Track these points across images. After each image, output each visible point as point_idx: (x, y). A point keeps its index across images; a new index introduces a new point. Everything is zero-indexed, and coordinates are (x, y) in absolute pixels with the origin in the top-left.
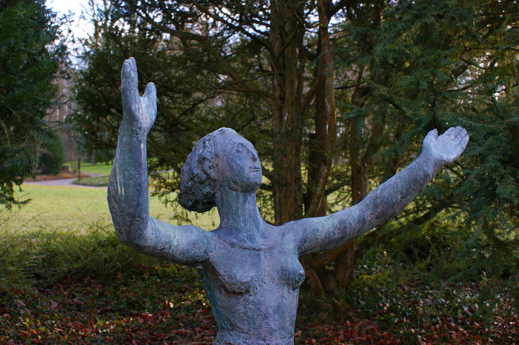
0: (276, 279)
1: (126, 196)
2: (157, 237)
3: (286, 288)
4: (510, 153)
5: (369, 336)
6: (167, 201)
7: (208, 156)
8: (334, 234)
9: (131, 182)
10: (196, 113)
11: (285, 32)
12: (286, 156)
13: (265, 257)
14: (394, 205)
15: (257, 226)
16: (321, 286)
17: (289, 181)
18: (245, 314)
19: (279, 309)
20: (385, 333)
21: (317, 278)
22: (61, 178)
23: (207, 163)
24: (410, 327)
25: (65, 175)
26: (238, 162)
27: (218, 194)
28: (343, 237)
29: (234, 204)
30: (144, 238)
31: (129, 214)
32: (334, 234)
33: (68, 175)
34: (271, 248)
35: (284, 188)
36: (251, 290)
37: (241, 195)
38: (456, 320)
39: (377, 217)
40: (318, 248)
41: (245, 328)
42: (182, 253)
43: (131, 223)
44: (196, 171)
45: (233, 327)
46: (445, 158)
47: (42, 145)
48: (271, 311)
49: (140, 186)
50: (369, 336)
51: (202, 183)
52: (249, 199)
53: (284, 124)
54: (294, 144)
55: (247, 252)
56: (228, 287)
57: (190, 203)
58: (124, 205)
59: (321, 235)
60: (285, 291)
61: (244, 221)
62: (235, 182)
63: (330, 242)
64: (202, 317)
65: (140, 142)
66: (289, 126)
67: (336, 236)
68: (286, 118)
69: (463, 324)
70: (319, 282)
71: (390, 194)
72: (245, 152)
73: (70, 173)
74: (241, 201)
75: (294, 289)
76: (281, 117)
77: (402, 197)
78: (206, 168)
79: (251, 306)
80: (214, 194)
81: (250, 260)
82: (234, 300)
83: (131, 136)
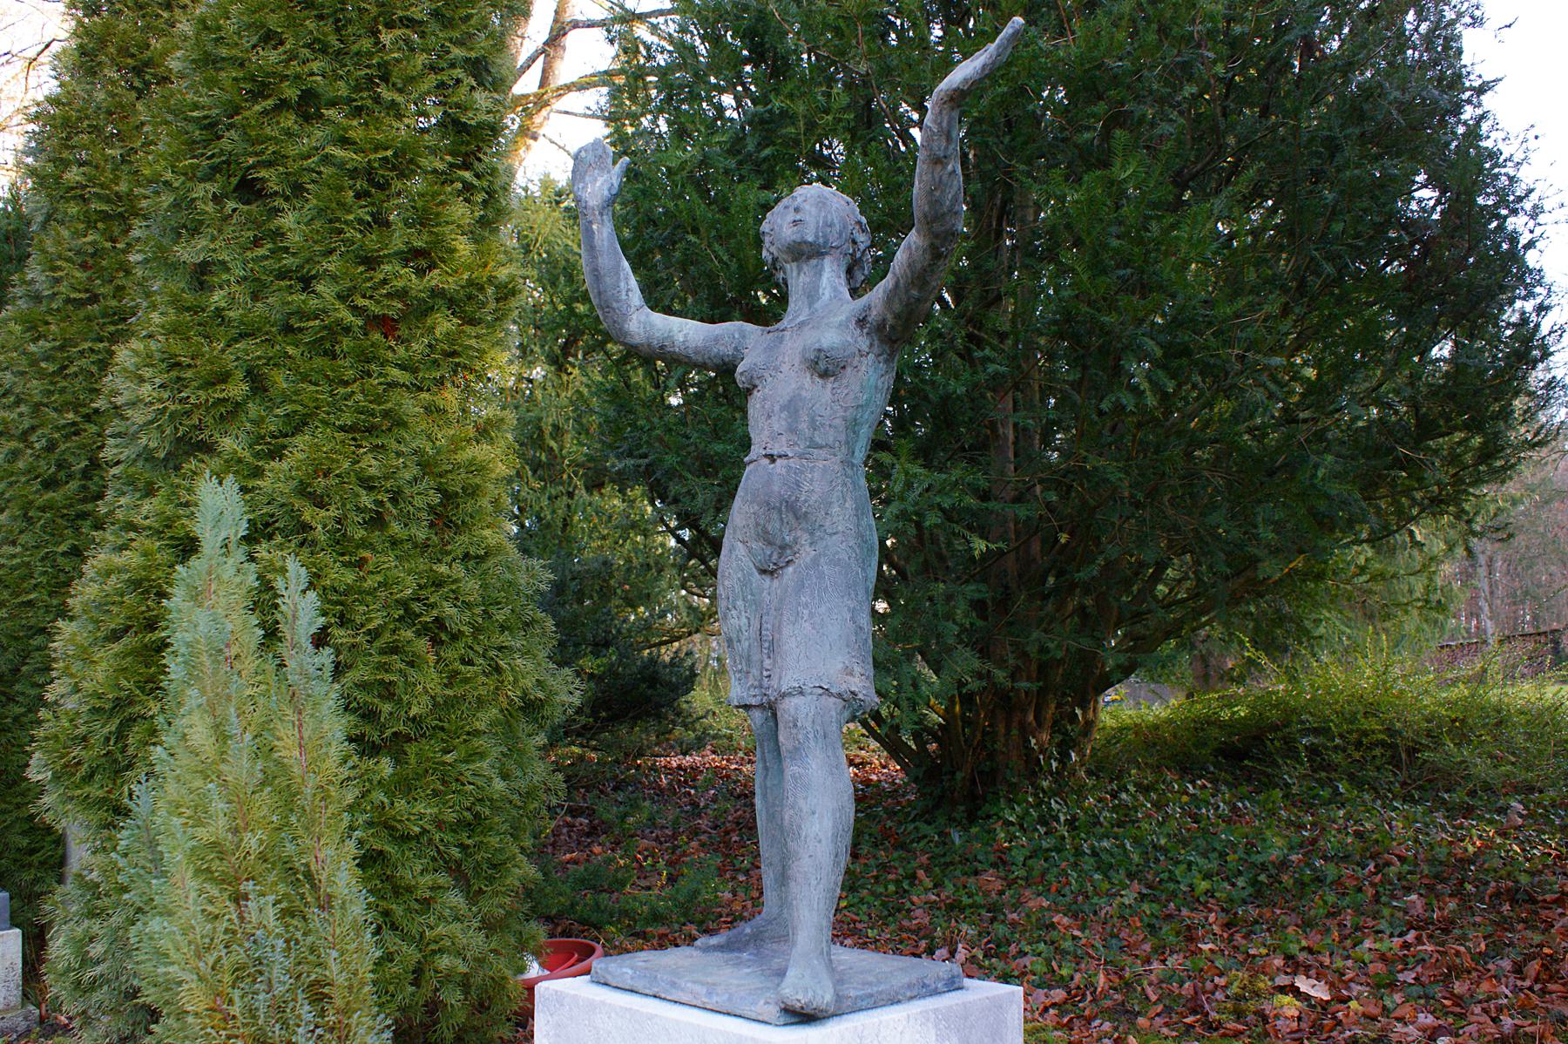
36: (757, 382)
37: (794, 265)
52: (805, 268)
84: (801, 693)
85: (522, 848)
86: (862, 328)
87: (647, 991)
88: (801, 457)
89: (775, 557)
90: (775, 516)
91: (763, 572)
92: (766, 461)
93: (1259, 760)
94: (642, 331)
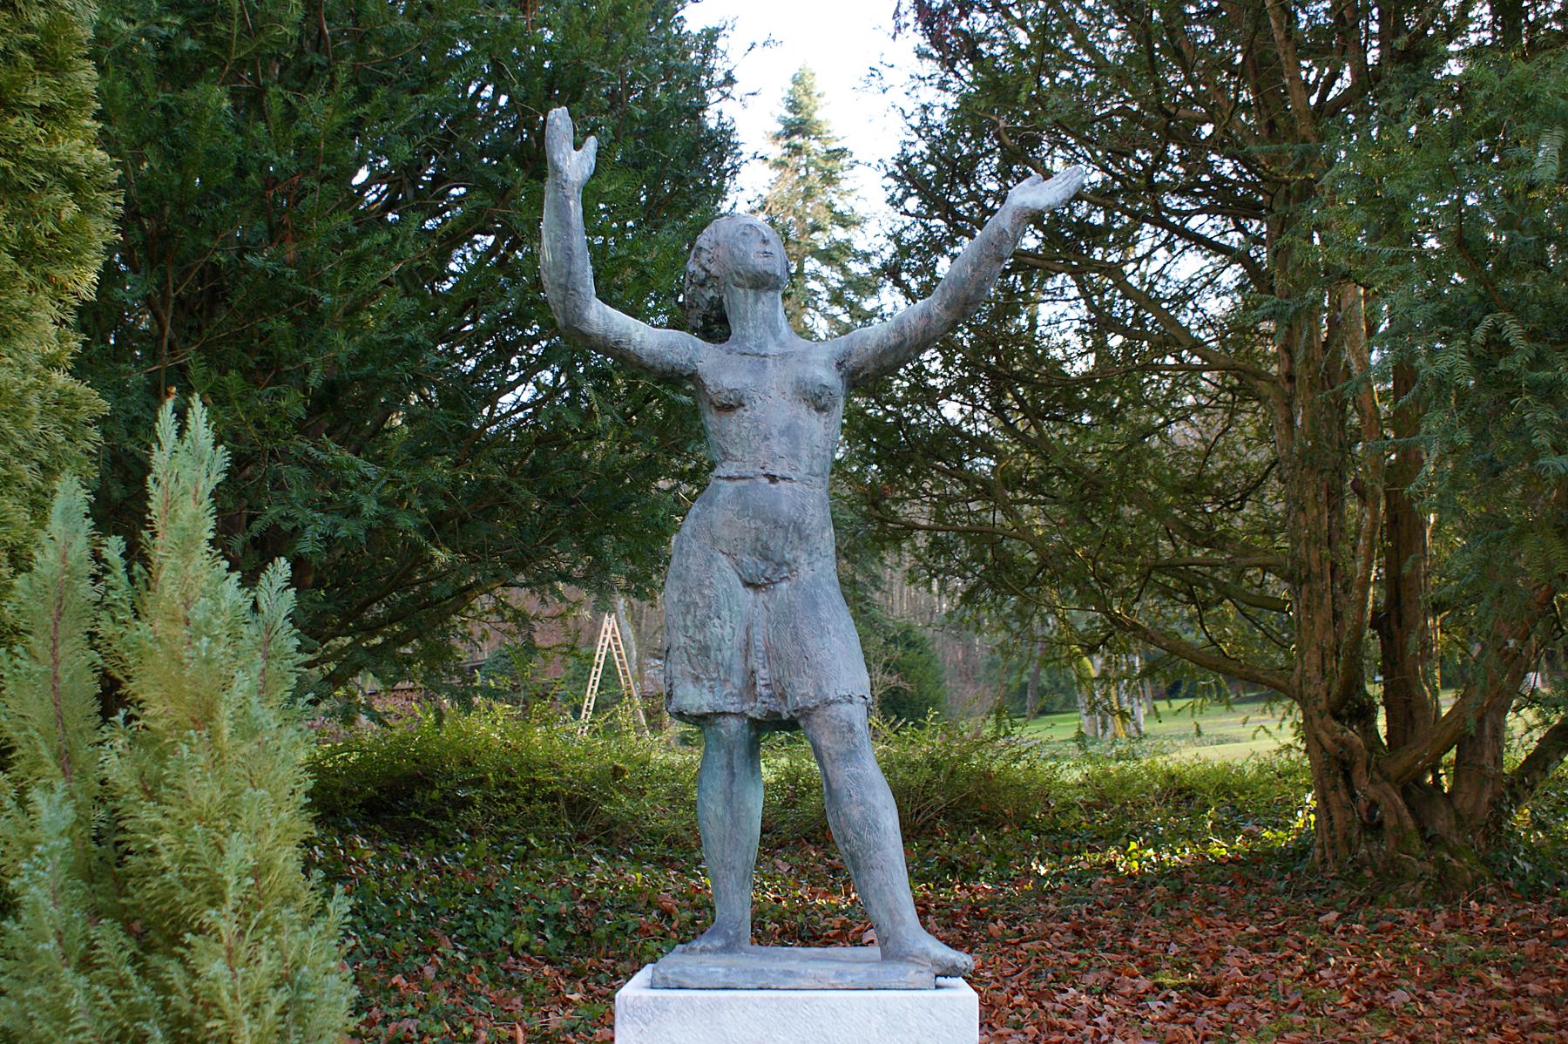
0: (789, 393)
1: (554, 263)
2: (605, 324)
3: (804, 407)
8: (889, 339)
9: (559, 244)
12: (1303, 509)
13: (775, 365)
15: (775, 332)
16: (1410, 823)
17: (1316, 569)
21: (1400, 802)
23: (704, 255)
26: (741, 246)
28: (902, 343)
30: (585, 320)
31: (560, 286)
32: (889, 339)
34: (784, 356)
35: (1304, 587)
36: (746, 402)
37: (751, 293)
39: (947, 308)
40: (872, 366)
41: (739, 454)
47: (886, 665)
48: (775, 432)
49: (570, 249)
52: (764, 298)
53: (1297, 434)
54: (1322, 480)
59: (871, 344)
61: (755, 327)
63: (885, 353)
65: (568, 198)
66: (1307, 439)
67: (892, 342)
68: (1299, 422)
70: (1405, 812)
74: (751, 300)
76: (1290, 421)
77: (973, 270)
78: (703, 262)
79: (746, 424)
80: (721, 299)
82: (725, 417)
84: (851, 702)
85: (54, 687)
86: (839, 369)
87: (749, 986)
88: (802, 482)
89: (769, 572)
90: (780, 533)
91: (747, 584)
92: (766, 481)
93: (1387, 796)
94: (601, 322)
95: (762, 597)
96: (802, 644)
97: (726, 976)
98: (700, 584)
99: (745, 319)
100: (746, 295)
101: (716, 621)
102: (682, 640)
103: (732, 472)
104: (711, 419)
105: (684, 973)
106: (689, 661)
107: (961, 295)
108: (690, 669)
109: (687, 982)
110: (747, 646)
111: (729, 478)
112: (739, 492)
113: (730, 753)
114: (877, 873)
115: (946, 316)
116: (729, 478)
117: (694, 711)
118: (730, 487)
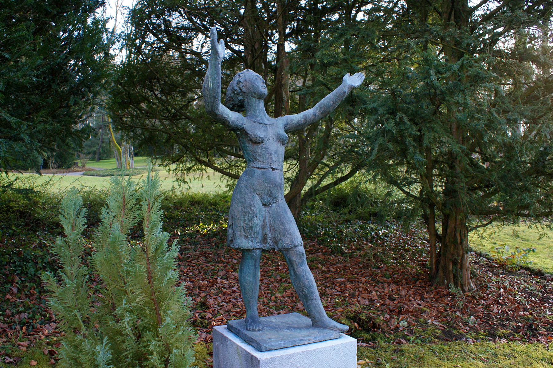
1: (213, 88)
4: (392, 107)
5: (312, 248)
6: (169, 170)
7: (242, 81)
10: (189, 108)
11: (255, 49)
14: (329, 107)
18: (261, 153)
19: (276, 152)
20: (322, 246)
22: (72, 172)
23: (241, 84)
24: (337, 243)
25: (76, 169)
27: (246, 100)
29: (254, 104)
30: (218, 110)
33: (79, 169)
37: (257, 100)
38: (367, 239)
39: (322, 113)
40: (294, 129)
41: (261, 160)
42: (232, 122)
43: (214, 101)
44: (236, 88)
45: (256, 159)
46: (353, 84)
50: (312, 248)
51: (238, 94)
55: (261, 125)
56: (253, 140)
57: (231, 106)
58: (211, 92)
59: (295, 122)
60: (279, 145)
62: (255, 93)
63: (299, 125)
64: (200, 239)
67: (302, 122)
69: (371, 242)
71: (328, 102)
72: (259, 79)
73: (80, 167)
74: (257, 103)
75: (283, 145)
81: (263, 128)
82: (256, 146)
83: (216, 61)
91: (263, 205)
95: (267, 209)
96: (284, 226)
97: (284, 344)
98: (251, 205)
99: (255, 109)
100: (256, 101)
101: (255, 218)
102: (242, 224)
103: (260, 166)
104: (249, 146)
105: (272, 345)
106: (244, 231)
107: (328, 110)
108: (244, 234)
109: (273, 348)
110: (264, 226)
111: (258, 168)
112: (263, 174)
113: (256, 261)
114: (314, 301)
115: (321, 116)
116: (258, 168)
117: (246, 248)
118: (259, 171)
